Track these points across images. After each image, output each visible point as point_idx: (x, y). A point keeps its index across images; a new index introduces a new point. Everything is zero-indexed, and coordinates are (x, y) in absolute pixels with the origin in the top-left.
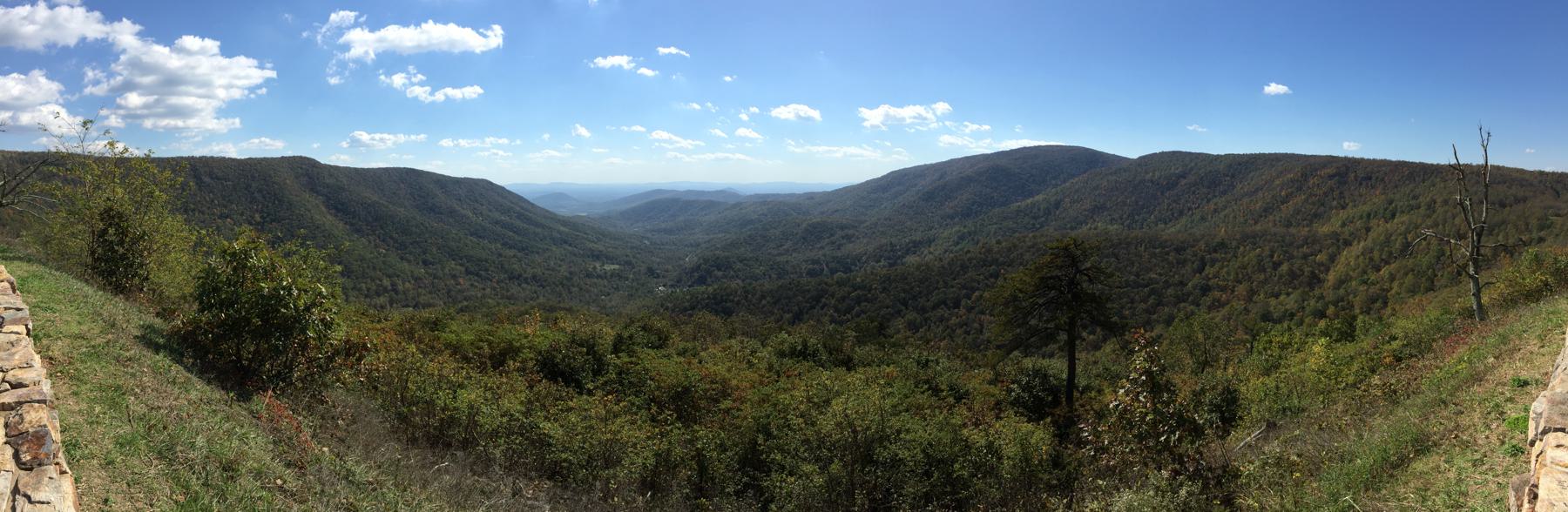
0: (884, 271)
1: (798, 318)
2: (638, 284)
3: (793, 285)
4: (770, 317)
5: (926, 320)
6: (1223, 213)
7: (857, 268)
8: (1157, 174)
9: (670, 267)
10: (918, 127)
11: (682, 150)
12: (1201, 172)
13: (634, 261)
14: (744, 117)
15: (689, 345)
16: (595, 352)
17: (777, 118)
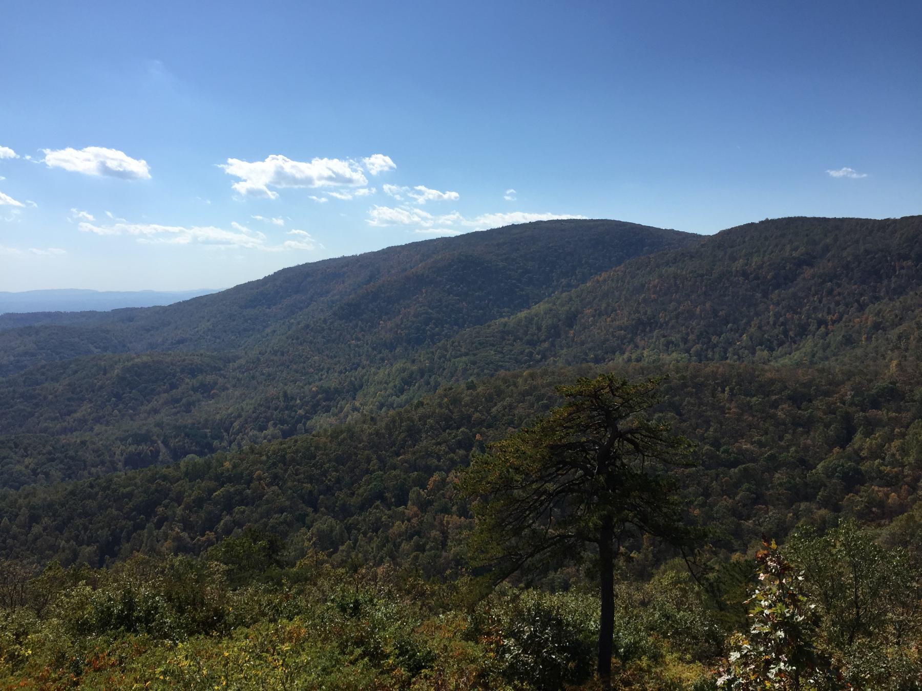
0: (274, 446)
4: (49, 557)
6: (897, 331)
7: (225, 444)
8: (756, 260)
10: (335, 194)
12: (845, 254)
17: (59, 170)
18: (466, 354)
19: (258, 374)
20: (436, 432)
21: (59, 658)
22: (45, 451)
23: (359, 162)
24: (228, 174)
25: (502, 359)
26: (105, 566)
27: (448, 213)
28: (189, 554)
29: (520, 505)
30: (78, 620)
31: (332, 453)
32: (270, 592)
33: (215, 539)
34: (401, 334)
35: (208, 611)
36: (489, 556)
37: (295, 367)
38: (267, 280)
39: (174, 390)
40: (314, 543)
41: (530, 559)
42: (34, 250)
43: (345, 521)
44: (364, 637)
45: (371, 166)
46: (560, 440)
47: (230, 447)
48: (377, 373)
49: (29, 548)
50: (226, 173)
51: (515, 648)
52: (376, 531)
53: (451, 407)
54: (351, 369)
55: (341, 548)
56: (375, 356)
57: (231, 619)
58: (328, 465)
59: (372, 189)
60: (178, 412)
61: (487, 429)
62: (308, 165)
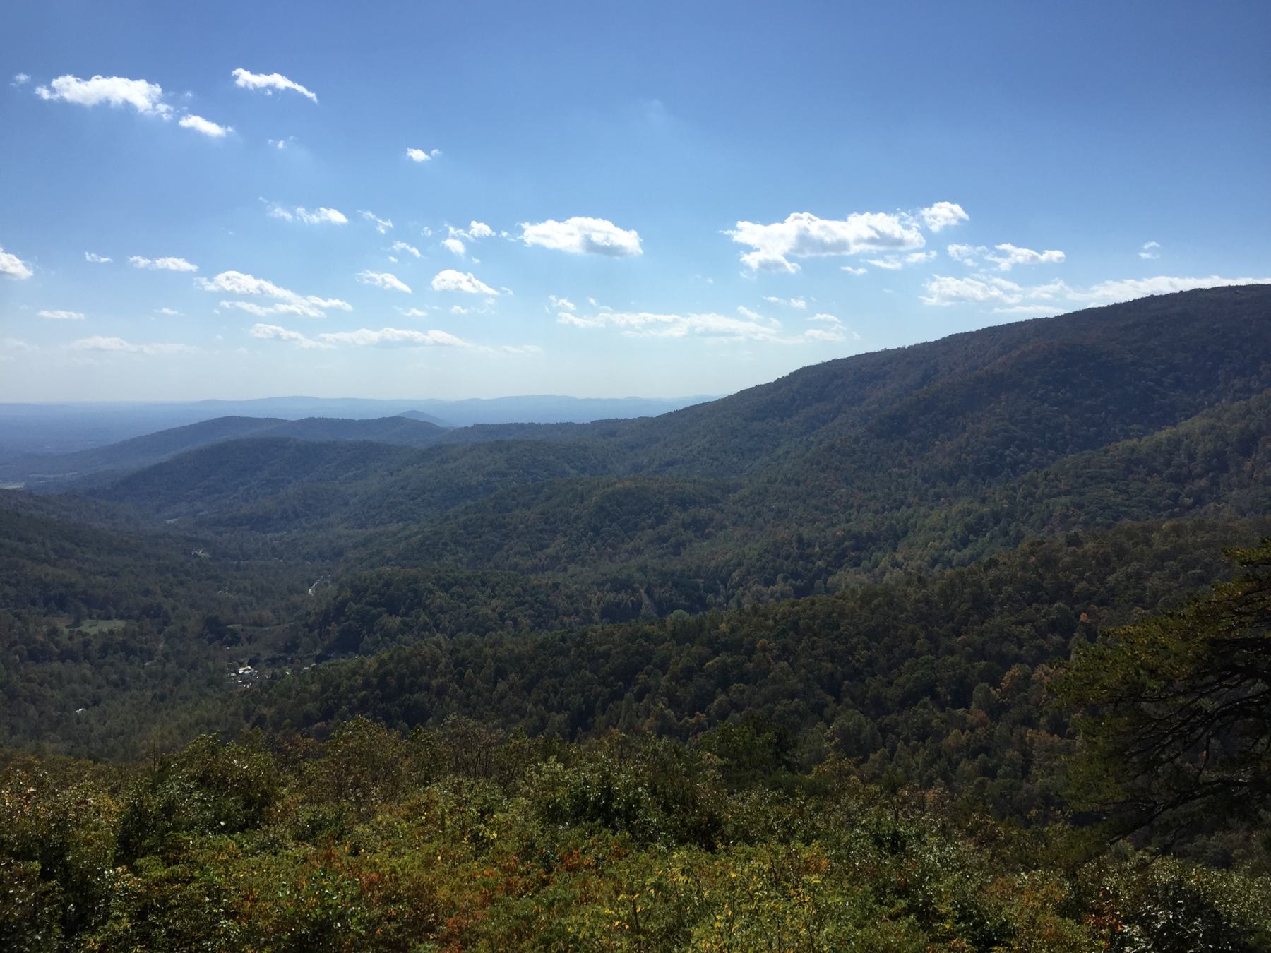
1: (580, 725)
2: (181, 665)
3: (569, 643)
4: (515, 722)
5: (884, 731)
7: (720, 599)
9: (267, 614)
10: (878, 263)
11: (290, 320)
13: (167, 605)
14: (455, 246)
15: (328, 810)
16: (67, 867)
17: (538, 248)
18: (1067, 493)
19: (765, 509)
20: (1016, 606)
21: (527, 847)
22: (513, 592)
23: (913, 215)
24: (736, 242)
25: (1127, 503)
26: (576, 740)
27: (1048, 283)
28: (674, 737)
29: (1155, 727)
30: (548, 804)
31: (862, 624)
32: (779, 802)
33: (706, 723)
34: (966, 460)
35: (702, 815)
36: (1101, 797)
37: (814, 502)
38: (781, 382)
39: (662, 526)
40: (836, 745)
41: (1170, 810)
42: (508, 348)
43: (879, 720)
44: (910, 886)
45: (932, 220)
46: (1228, 631)
47: (727, 604)
48: (929, 515)
49: (494, 708)
50: (734, 240)
51: (1142, 940)
52: (923, 738)
53: (1041, 571)
54: (892, 509)
55: (872, 756)
56: (927, 490)
57: (729, 829)
58: (855, 640)
59: (931, 252)
60: (665, 554)
61: (1099, 606)
62: (843, 224)
